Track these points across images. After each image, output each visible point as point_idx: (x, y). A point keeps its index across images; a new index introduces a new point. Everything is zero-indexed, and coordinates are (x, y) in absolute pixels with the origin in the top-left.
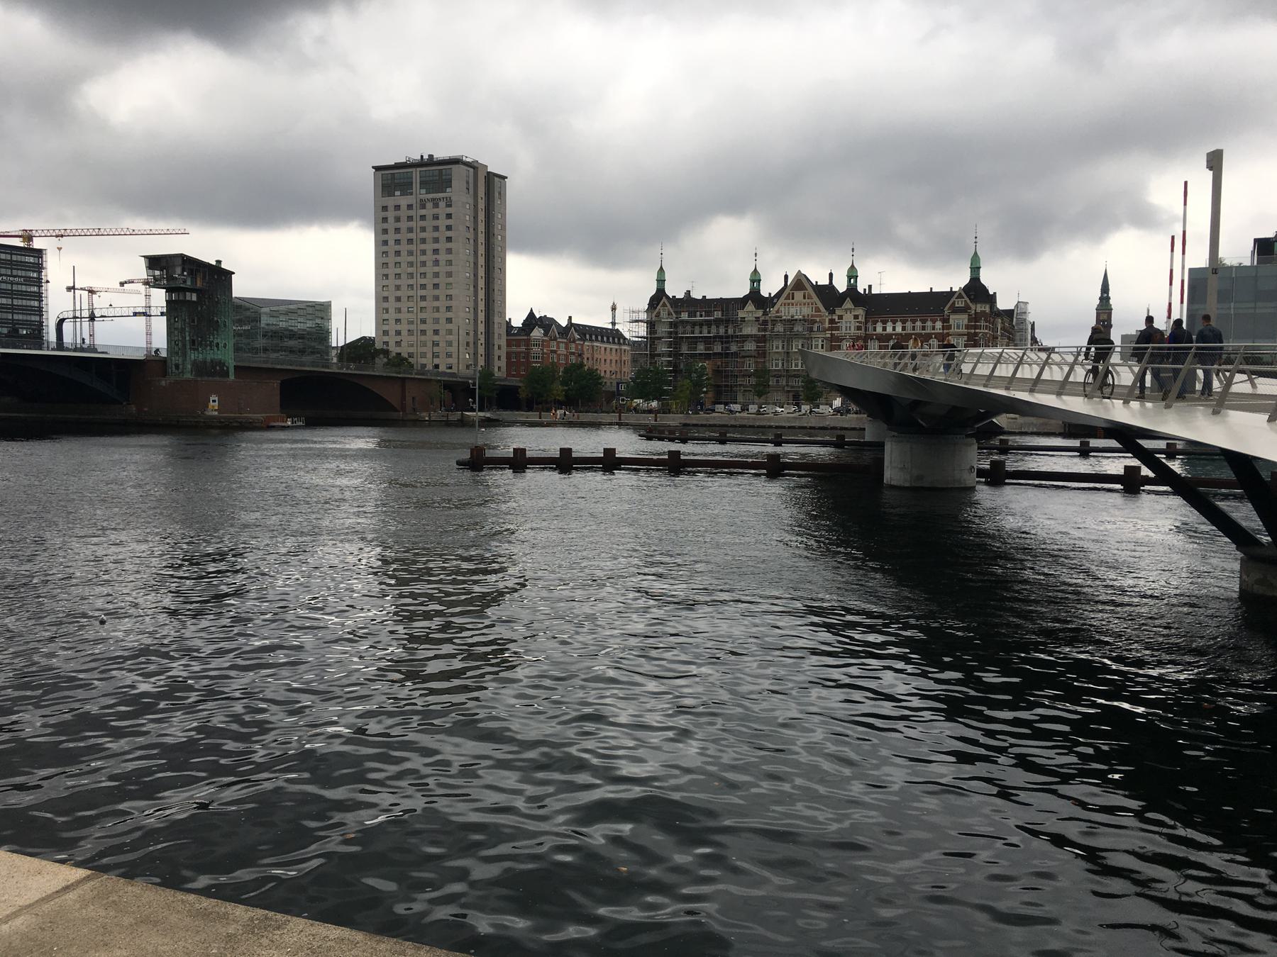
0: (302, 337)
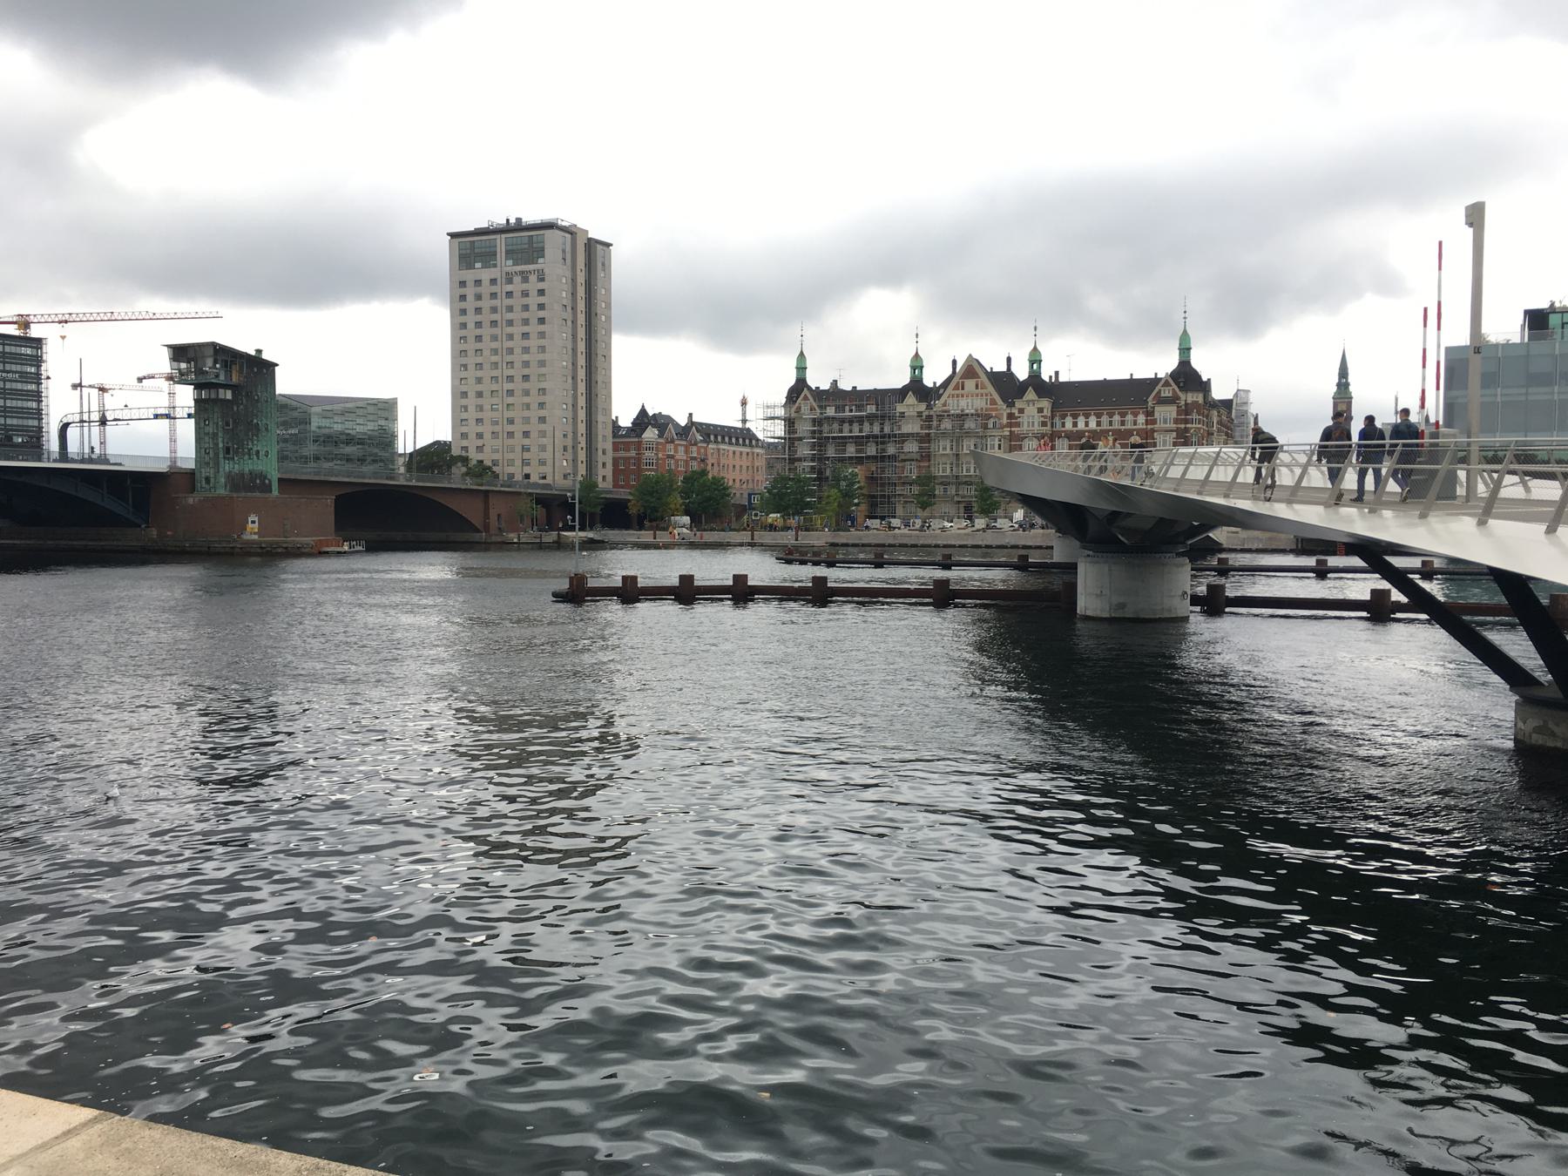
0: (361, 442)
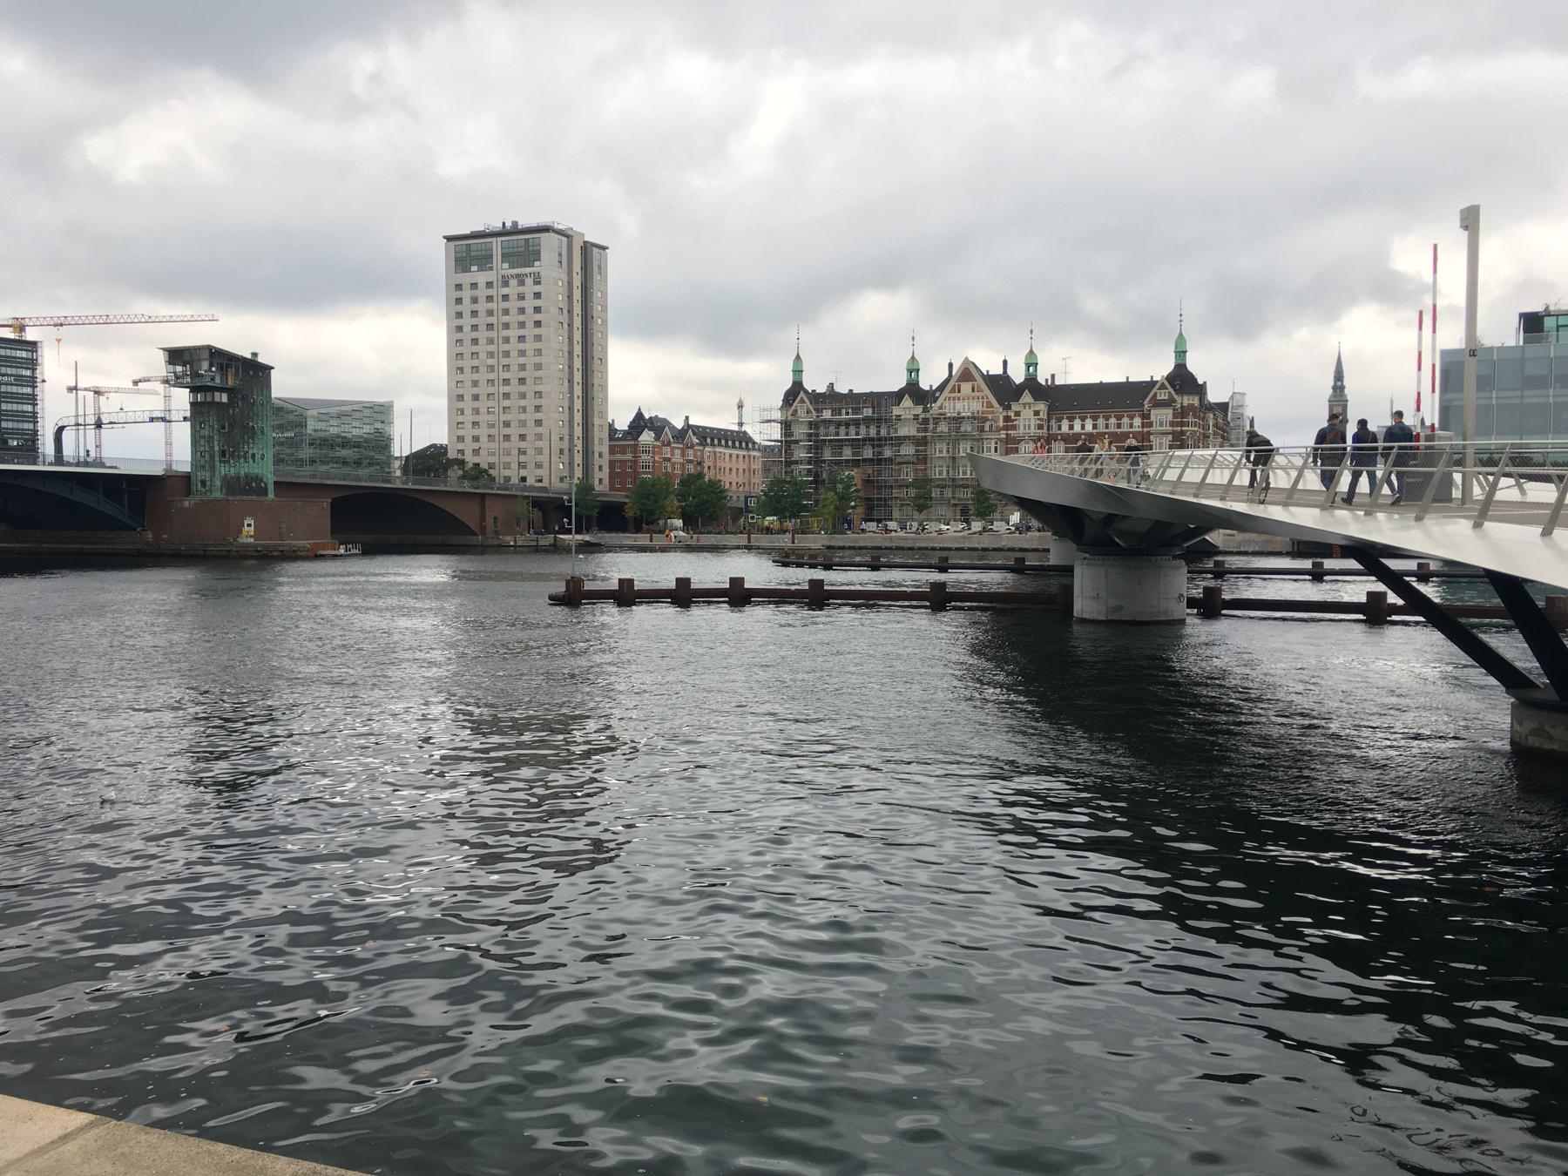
0: (357, 445)
